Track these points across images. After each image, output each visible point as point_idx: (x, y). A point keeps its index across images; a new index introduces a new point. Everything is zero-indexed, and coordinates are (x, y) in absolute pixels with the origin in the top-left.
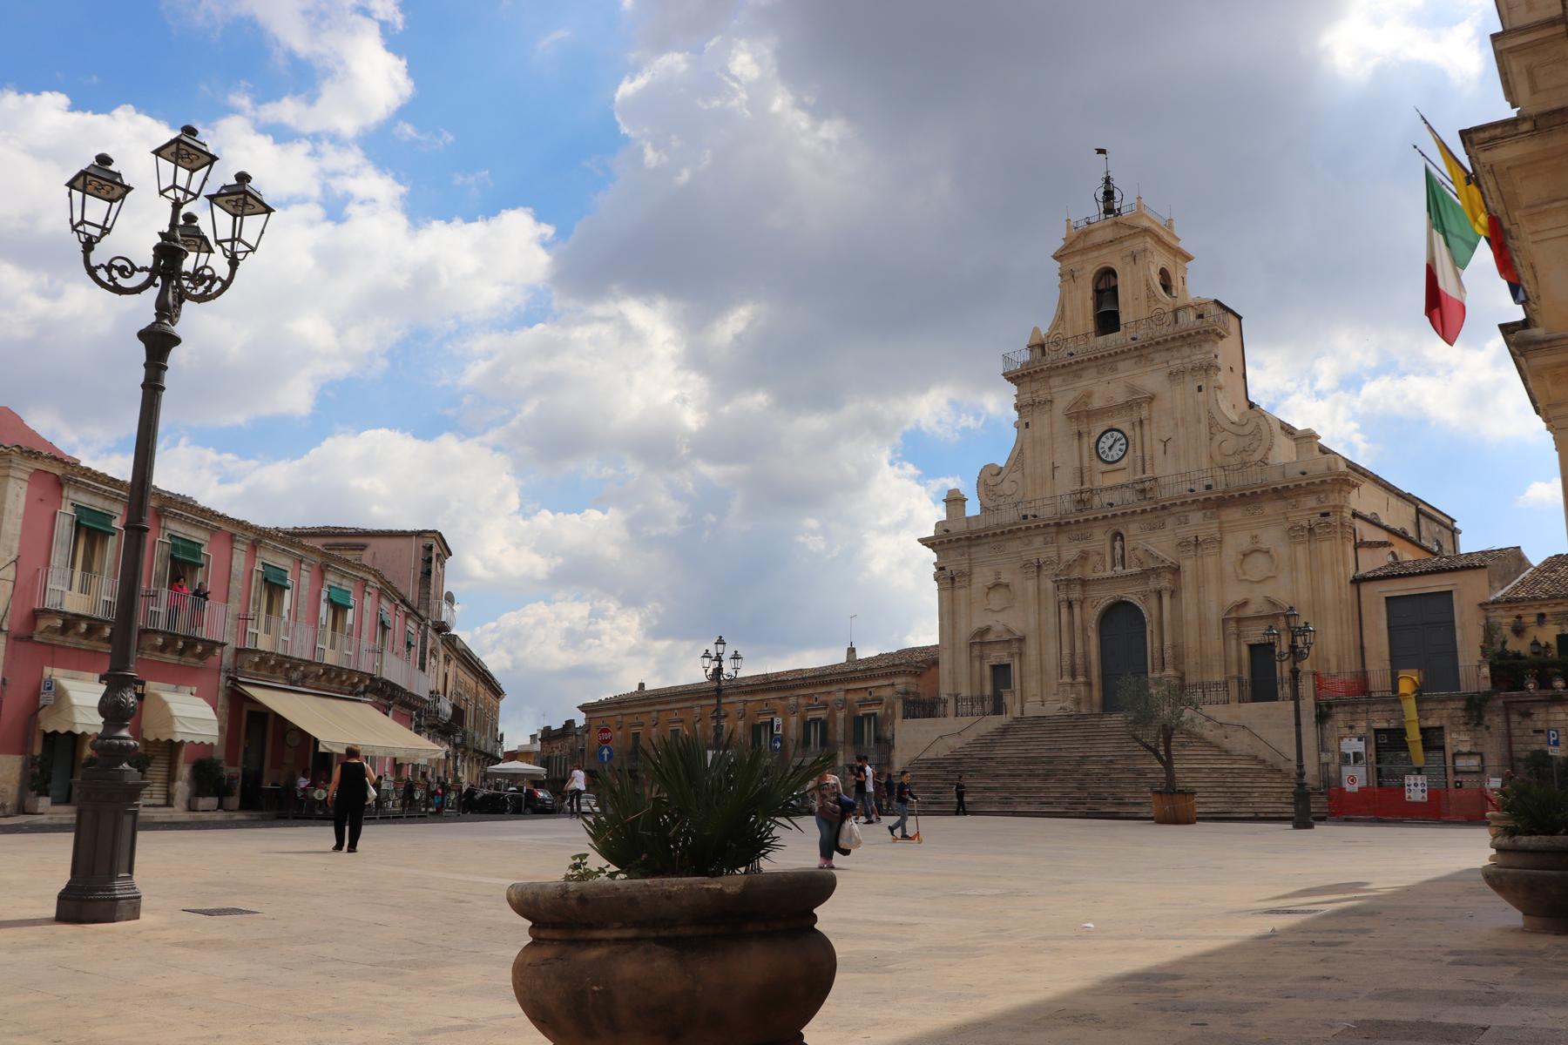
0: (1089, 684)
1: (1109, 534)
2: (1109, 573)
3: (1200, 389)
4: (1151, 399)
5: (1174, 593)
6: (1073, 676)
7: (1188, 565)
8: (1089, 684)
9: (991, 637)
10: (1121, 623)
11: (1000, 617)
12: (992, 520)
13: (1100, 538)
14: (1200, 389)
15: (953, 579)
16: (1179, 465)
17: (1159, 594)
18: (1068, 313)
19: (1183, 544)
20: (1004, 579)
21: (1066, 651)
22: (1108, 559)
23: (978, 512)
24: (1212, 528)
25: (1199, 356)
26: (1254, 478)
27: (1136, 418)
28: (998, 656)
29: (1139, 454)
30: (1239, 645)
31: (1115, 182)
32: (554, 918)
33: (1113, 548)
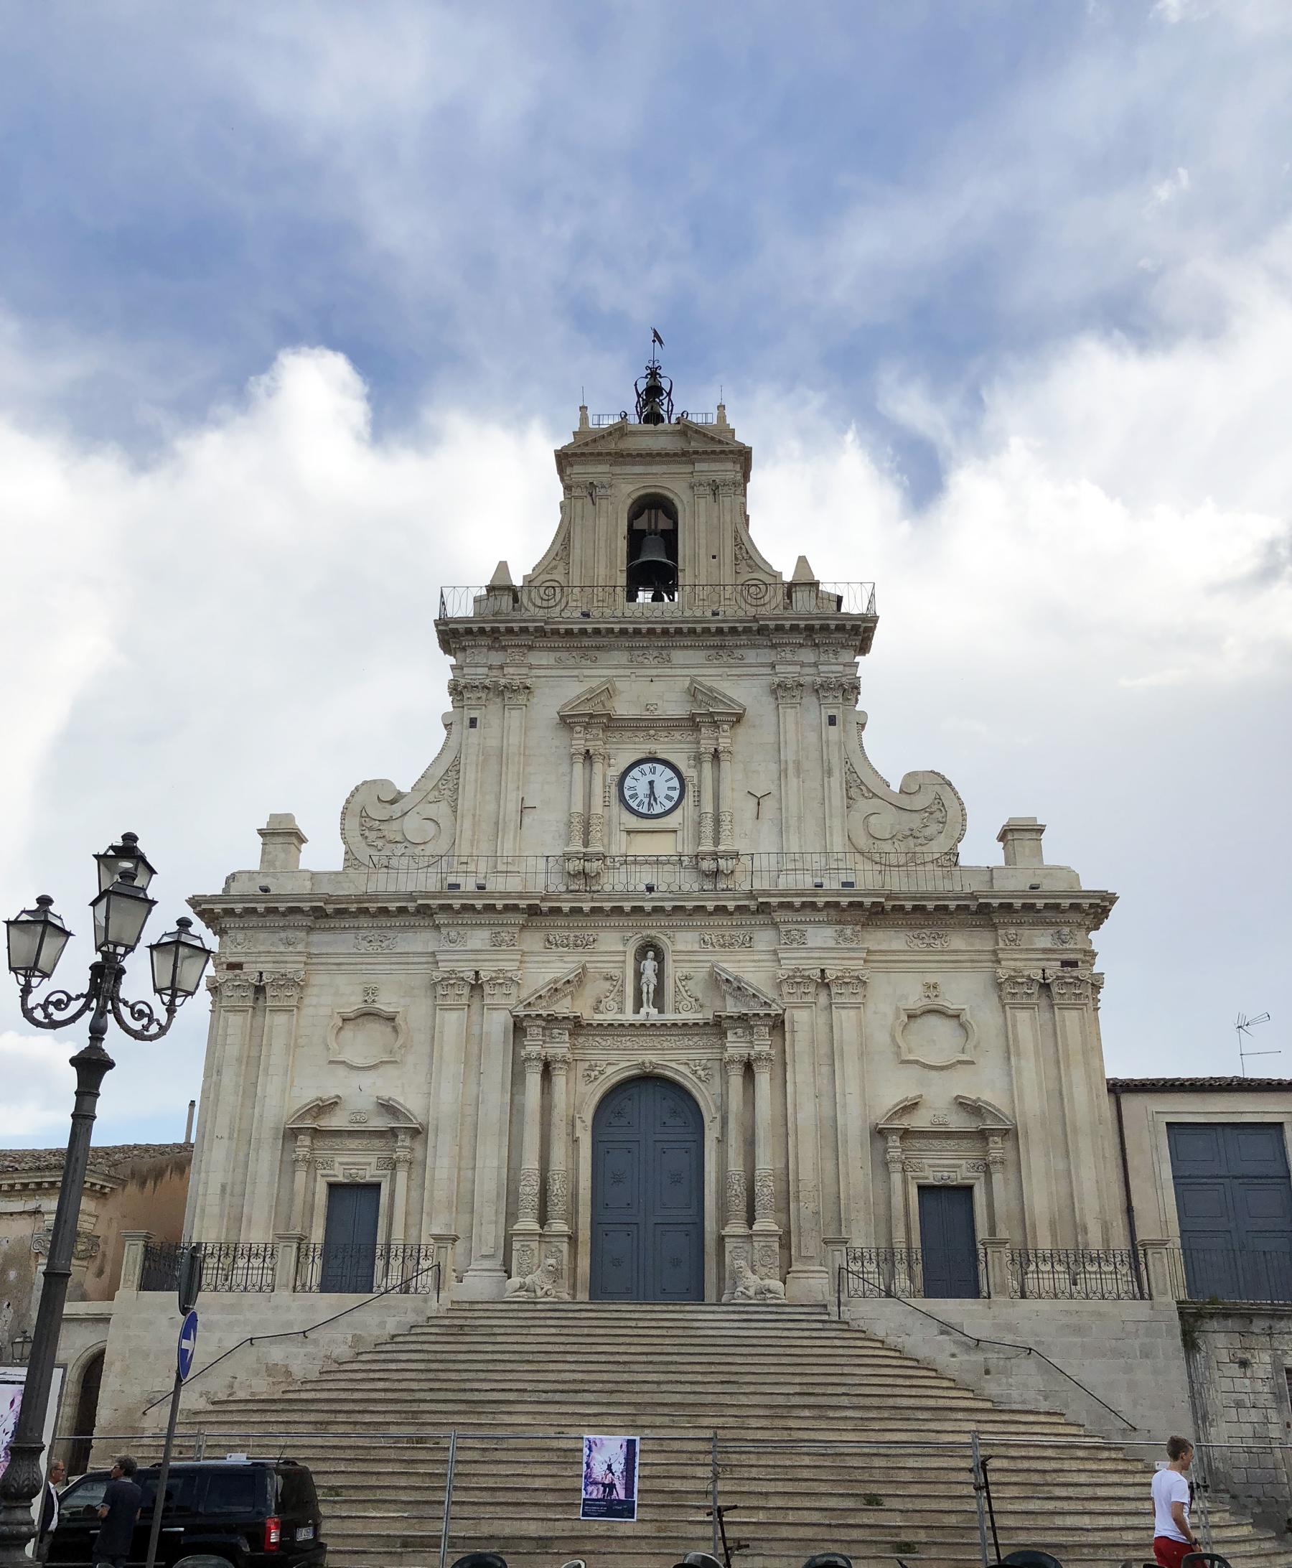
0: (573, 1239)
1: (631, 950)
2: (629, 1016)
3: (832, 720)
4: (738, 719)
6: (543, 1220)
7: (801, 1020)
8: (573, 1239)
10: (651, 1118)
11: (366, 1080)
12: (357, 885)
13: (613, 948)
14: (832, 720)
16: (776, 846)
17: (748, 1069)
19: (797, 980)
20: (386, 1003)
21: (531, 1163)
23: (337, 864)
25: (831, 669)
26: (927, 882)
27: (707, 745)
28: (358, 1163)
29: (708, 807)
30: (905, 1182)
33: (639, 974)
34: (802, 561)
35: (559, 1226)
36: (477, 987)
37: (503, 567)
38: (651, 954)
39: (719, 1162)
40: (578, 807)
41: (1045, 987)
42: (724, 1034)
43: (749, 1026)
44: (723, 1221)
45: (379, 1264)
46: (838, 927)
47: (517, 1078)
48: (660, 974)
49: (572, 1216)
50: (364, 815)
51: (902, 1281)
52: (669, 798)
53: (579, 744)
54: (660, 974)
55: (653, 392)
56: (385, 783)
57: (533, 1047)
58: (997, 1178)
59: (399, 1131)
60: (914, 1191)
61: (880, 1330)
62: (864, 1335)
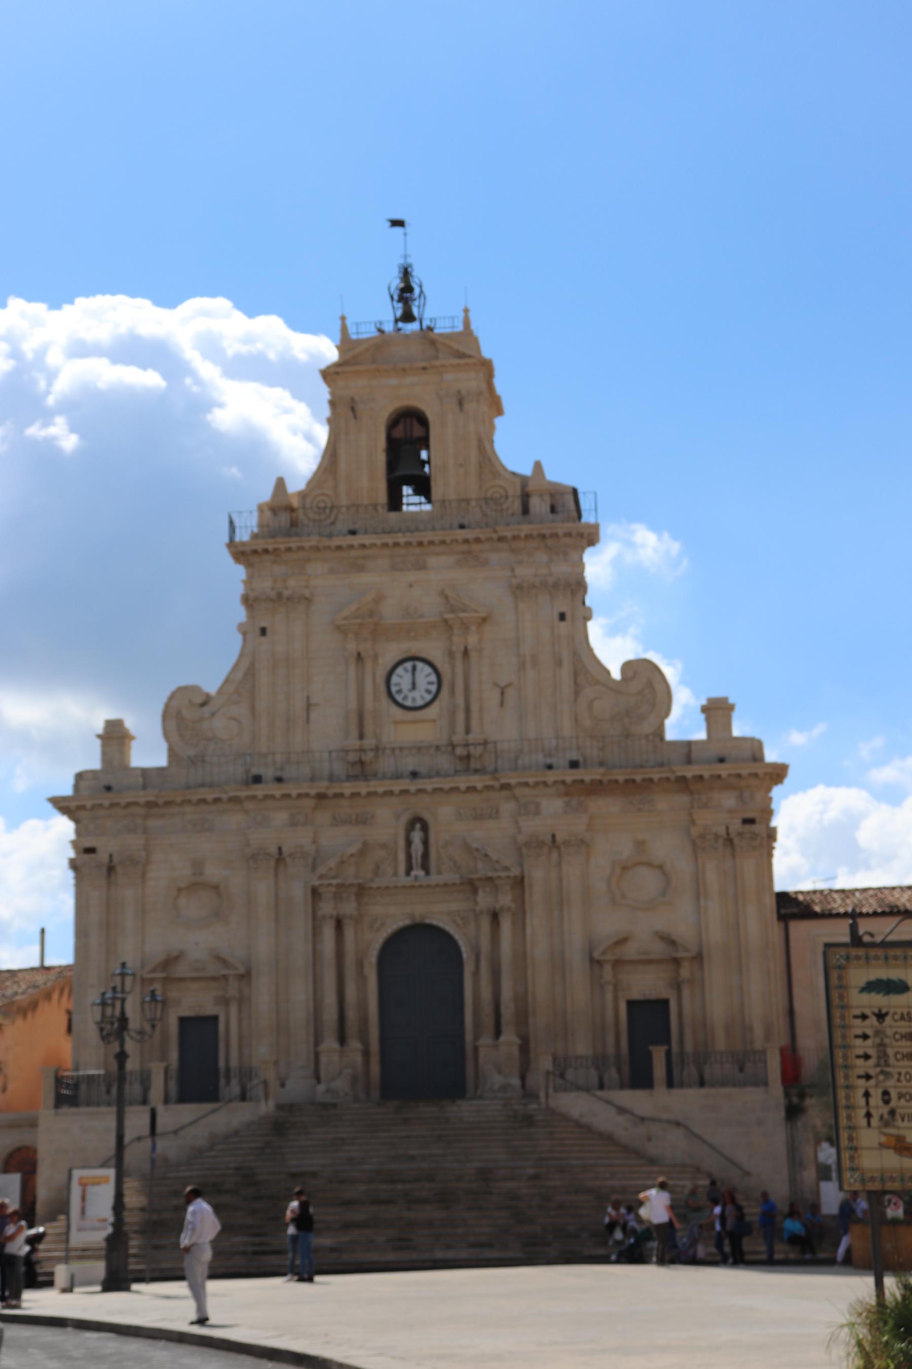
3: (562, 617)
5: (520, 913)
6: (342, 1039)
7: (539, 874)
9: (181, 970)
14: (562, 617)
15: (111, 869)
17: (495, 916)
18: (343, 466)
20: (212, 872)
22: (402, 857)
24: (135, 842)
27: (458, 643)
29: (460, 701)
30: (616, 999)
31: (418, 275)
32: (880, 1314)
33: (409, 842)
34: (538, 466)
35: (355, 1044)
36: (280, 858)
37: (280, 484)
38: (418, 826)
39: (474, 988)
40: (353, 705)
41: (729, 841)
42: (475, 891)
43: (502, 888)
44: (476, 1038)
45: (222, 1081)
46: (566, 799)
47: (316, 932)
48: (426, 842)
49: (364, 1038)
50: (179, 715)
51: (612, 1075)
52: (428, 692)
53: (352, 646)
54: (426, 842)
55: (406, 292)
56: (195, 689)
57: (327, 908)
58: (686, 992)
59: (235, 977)
60: (623, 1007)
61: (575, 1113)
62: (566, 1118)
